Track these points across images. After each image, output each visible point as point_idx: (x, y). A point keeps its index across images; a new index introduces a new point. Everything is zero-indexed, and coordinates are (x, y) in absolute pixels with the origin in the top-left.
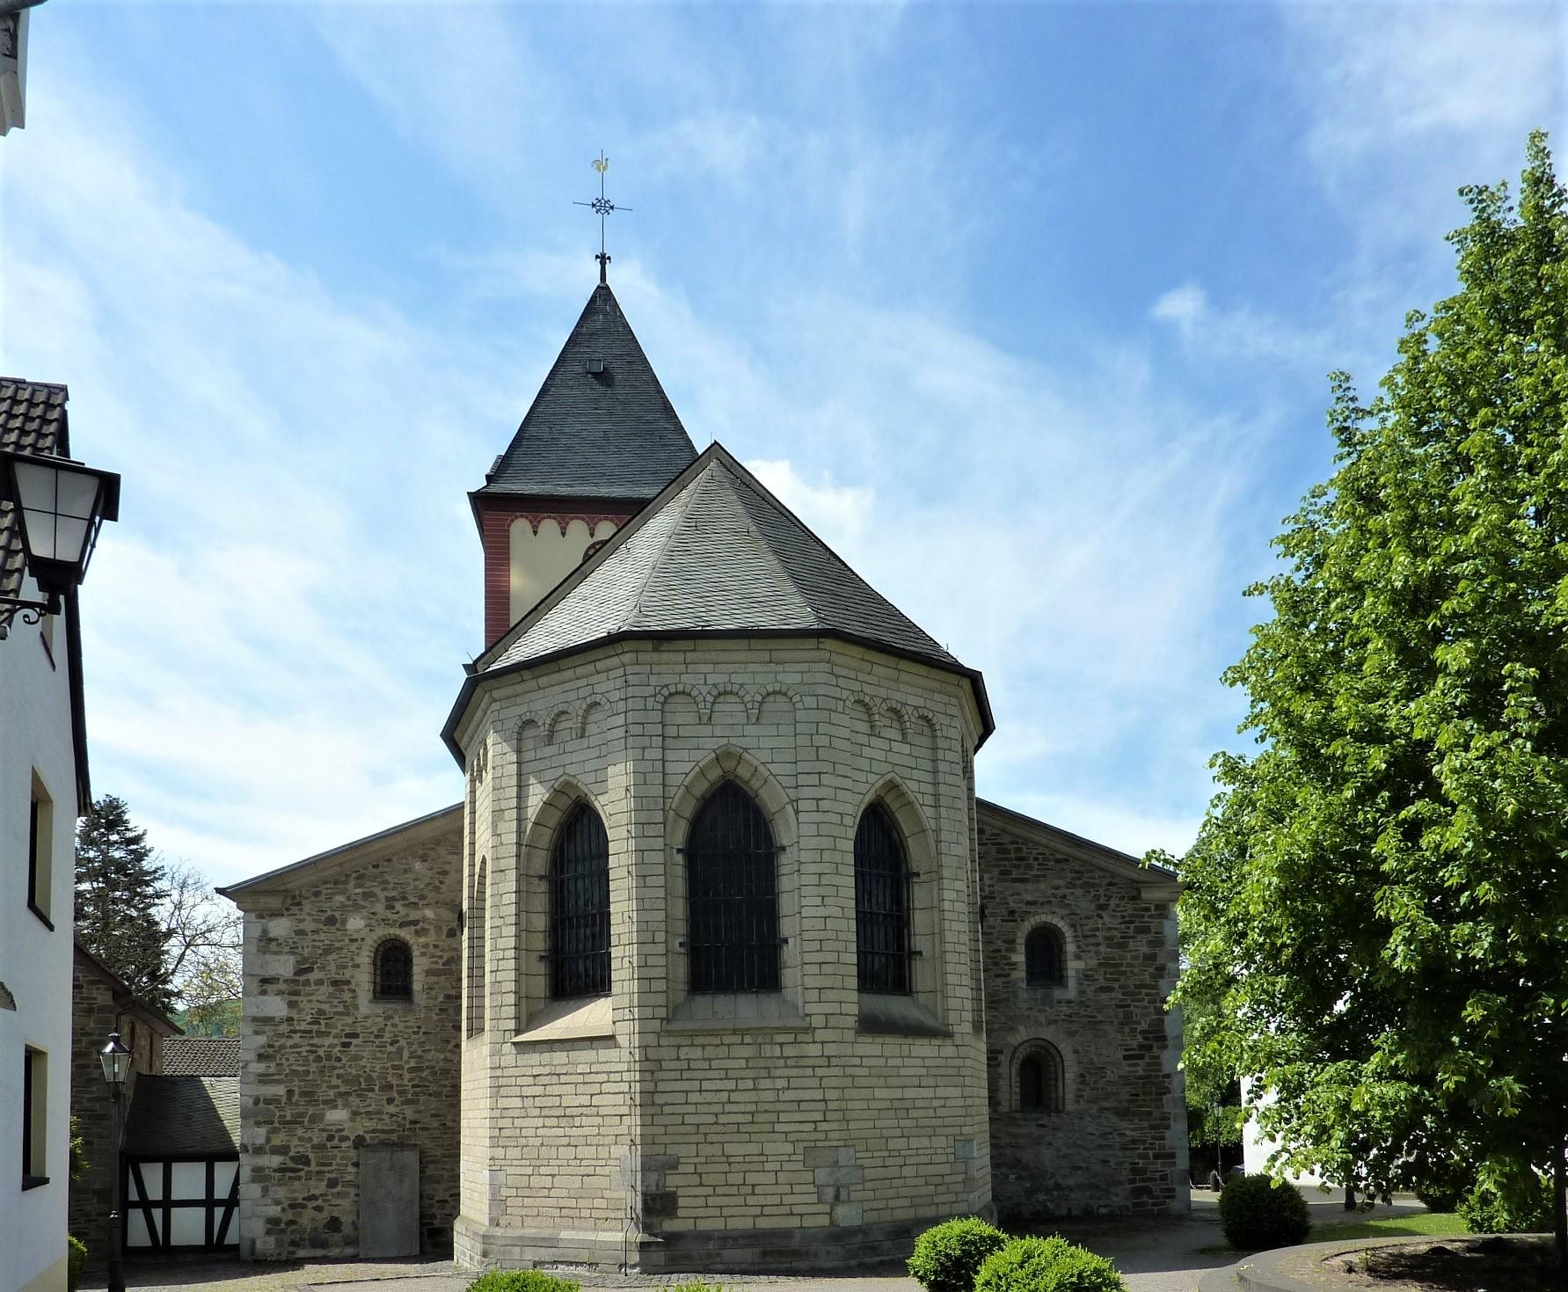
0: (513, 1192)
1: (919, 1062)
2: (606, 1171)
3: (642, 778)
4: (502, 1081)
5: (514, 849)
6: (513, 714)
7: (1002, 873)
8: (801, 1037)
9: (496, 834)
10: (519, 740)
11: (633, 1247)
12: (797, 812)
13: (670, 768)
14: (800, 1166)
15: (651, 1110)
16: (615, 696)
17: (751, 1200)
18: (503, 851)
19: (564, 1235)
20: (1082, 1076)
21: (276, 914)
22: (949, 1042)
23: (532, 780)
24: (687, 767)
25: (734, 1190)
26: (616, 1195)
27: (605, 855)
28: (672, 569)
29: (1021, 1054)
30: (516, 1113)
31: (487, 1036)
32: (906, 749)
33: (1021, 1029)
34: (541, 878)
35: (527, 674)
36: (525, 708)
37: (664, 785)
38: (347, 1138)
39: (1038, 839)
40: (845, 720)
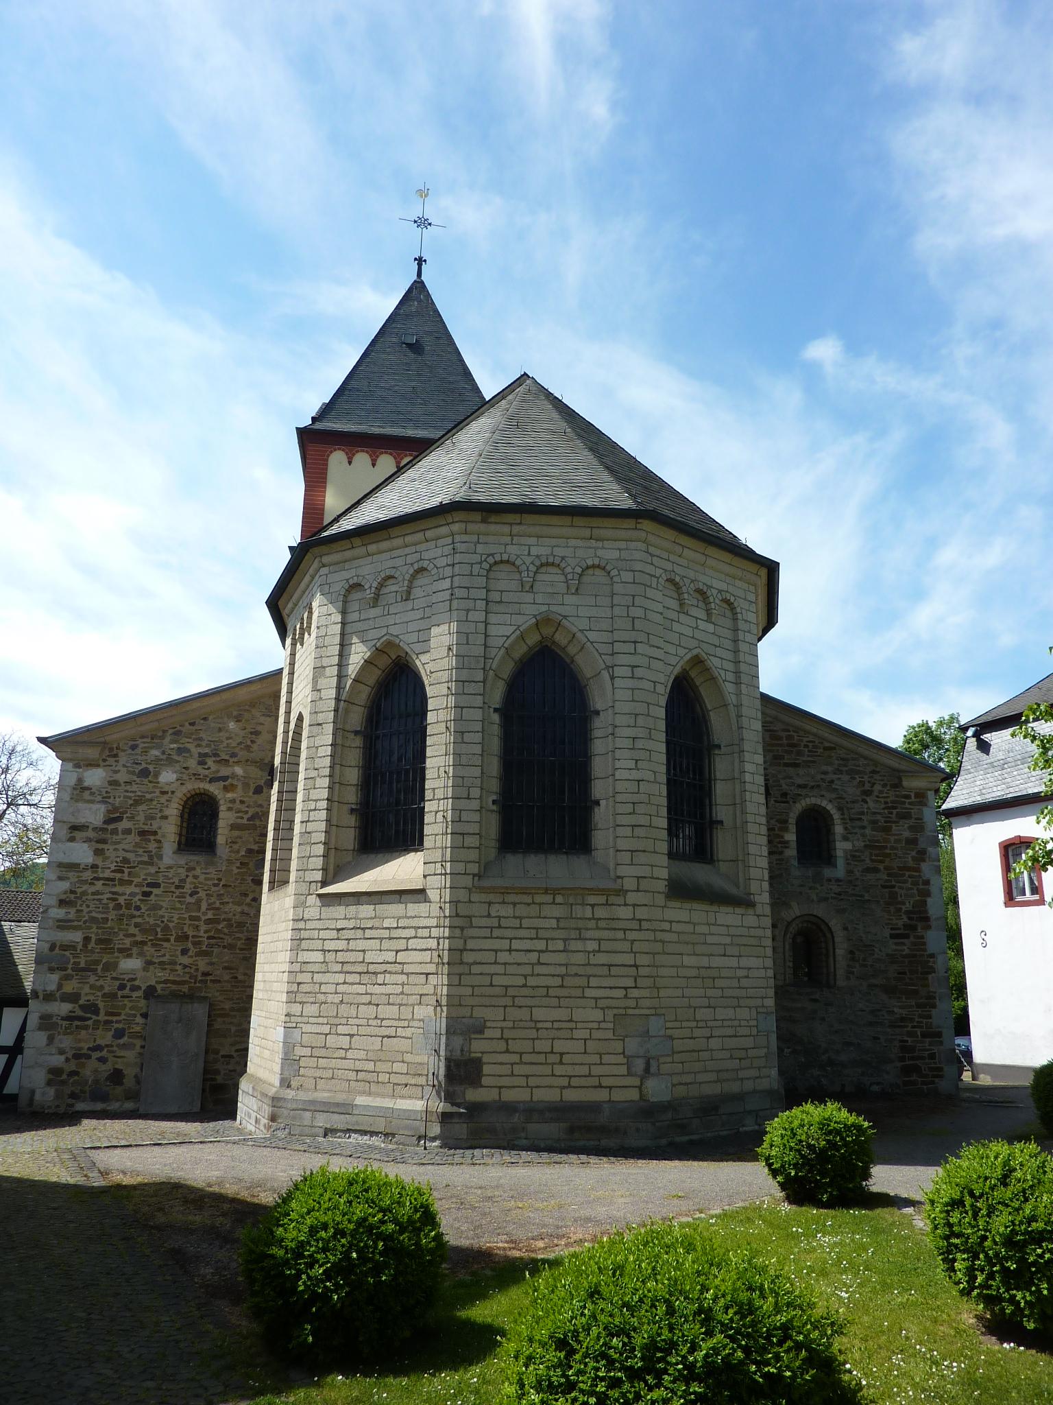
0: (307, 1052)
1: (723, 930)
2: (408, 1032)
3: (464, 638)
4: (304, 934)
5: (333, 703)
6: (340, 579)
7: (775, 757)
8: (612, 899)
9: (316, 689)
10: (345, 602)
11: (434, 1118)
12: (612, 678)
13: (493, 630)
14: (610, 1035)
15: (461, 969)
16: (442, 562)
17: (559, 1070)
18: (321, 706)
19: (360, 1100)
20: (851, 952)
21: (92, 764)
22: (751, 911)
23: (355, 640)
24: (508, 630)
25: (541, 1058)
26: (418, 1059)
27: (424, 712)
28: (496, 456)
29: (793, 929)
30: (316, 968)
31: (291, 888)
32: (711, 628)
33: (794, 904)
34: (356, 733)
35: (357, 541)
36: (353, 572)
37: (486, 646)
38: (139, 988)
39: (808, 727)
40: (658, 595)
